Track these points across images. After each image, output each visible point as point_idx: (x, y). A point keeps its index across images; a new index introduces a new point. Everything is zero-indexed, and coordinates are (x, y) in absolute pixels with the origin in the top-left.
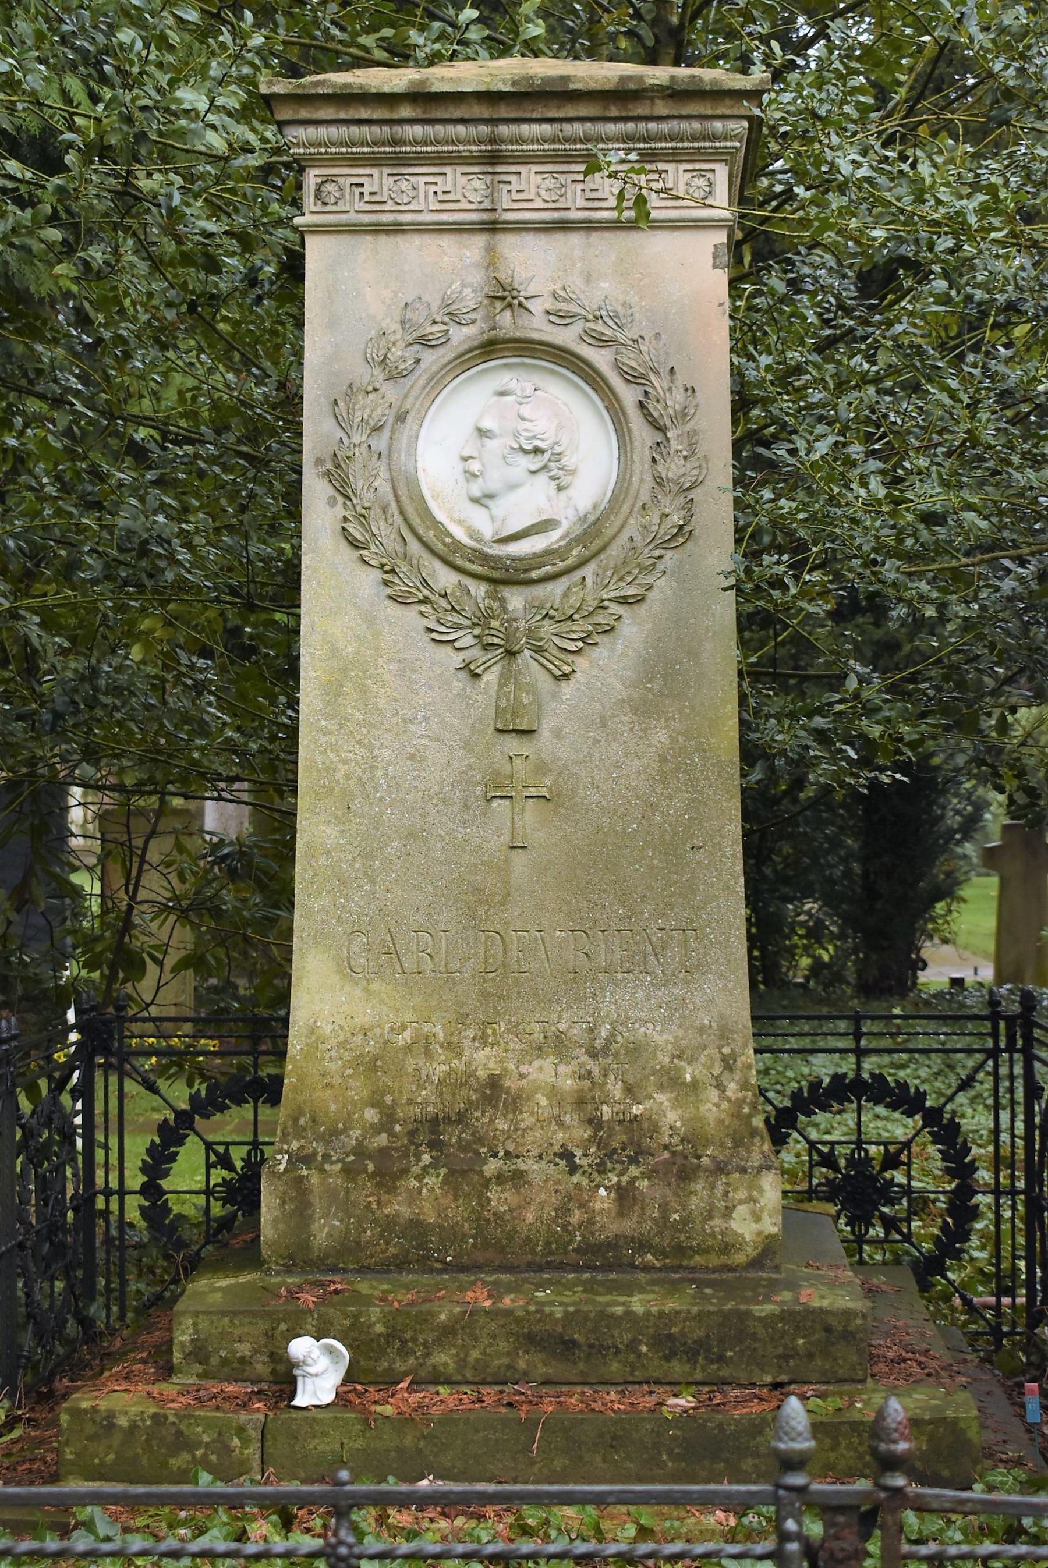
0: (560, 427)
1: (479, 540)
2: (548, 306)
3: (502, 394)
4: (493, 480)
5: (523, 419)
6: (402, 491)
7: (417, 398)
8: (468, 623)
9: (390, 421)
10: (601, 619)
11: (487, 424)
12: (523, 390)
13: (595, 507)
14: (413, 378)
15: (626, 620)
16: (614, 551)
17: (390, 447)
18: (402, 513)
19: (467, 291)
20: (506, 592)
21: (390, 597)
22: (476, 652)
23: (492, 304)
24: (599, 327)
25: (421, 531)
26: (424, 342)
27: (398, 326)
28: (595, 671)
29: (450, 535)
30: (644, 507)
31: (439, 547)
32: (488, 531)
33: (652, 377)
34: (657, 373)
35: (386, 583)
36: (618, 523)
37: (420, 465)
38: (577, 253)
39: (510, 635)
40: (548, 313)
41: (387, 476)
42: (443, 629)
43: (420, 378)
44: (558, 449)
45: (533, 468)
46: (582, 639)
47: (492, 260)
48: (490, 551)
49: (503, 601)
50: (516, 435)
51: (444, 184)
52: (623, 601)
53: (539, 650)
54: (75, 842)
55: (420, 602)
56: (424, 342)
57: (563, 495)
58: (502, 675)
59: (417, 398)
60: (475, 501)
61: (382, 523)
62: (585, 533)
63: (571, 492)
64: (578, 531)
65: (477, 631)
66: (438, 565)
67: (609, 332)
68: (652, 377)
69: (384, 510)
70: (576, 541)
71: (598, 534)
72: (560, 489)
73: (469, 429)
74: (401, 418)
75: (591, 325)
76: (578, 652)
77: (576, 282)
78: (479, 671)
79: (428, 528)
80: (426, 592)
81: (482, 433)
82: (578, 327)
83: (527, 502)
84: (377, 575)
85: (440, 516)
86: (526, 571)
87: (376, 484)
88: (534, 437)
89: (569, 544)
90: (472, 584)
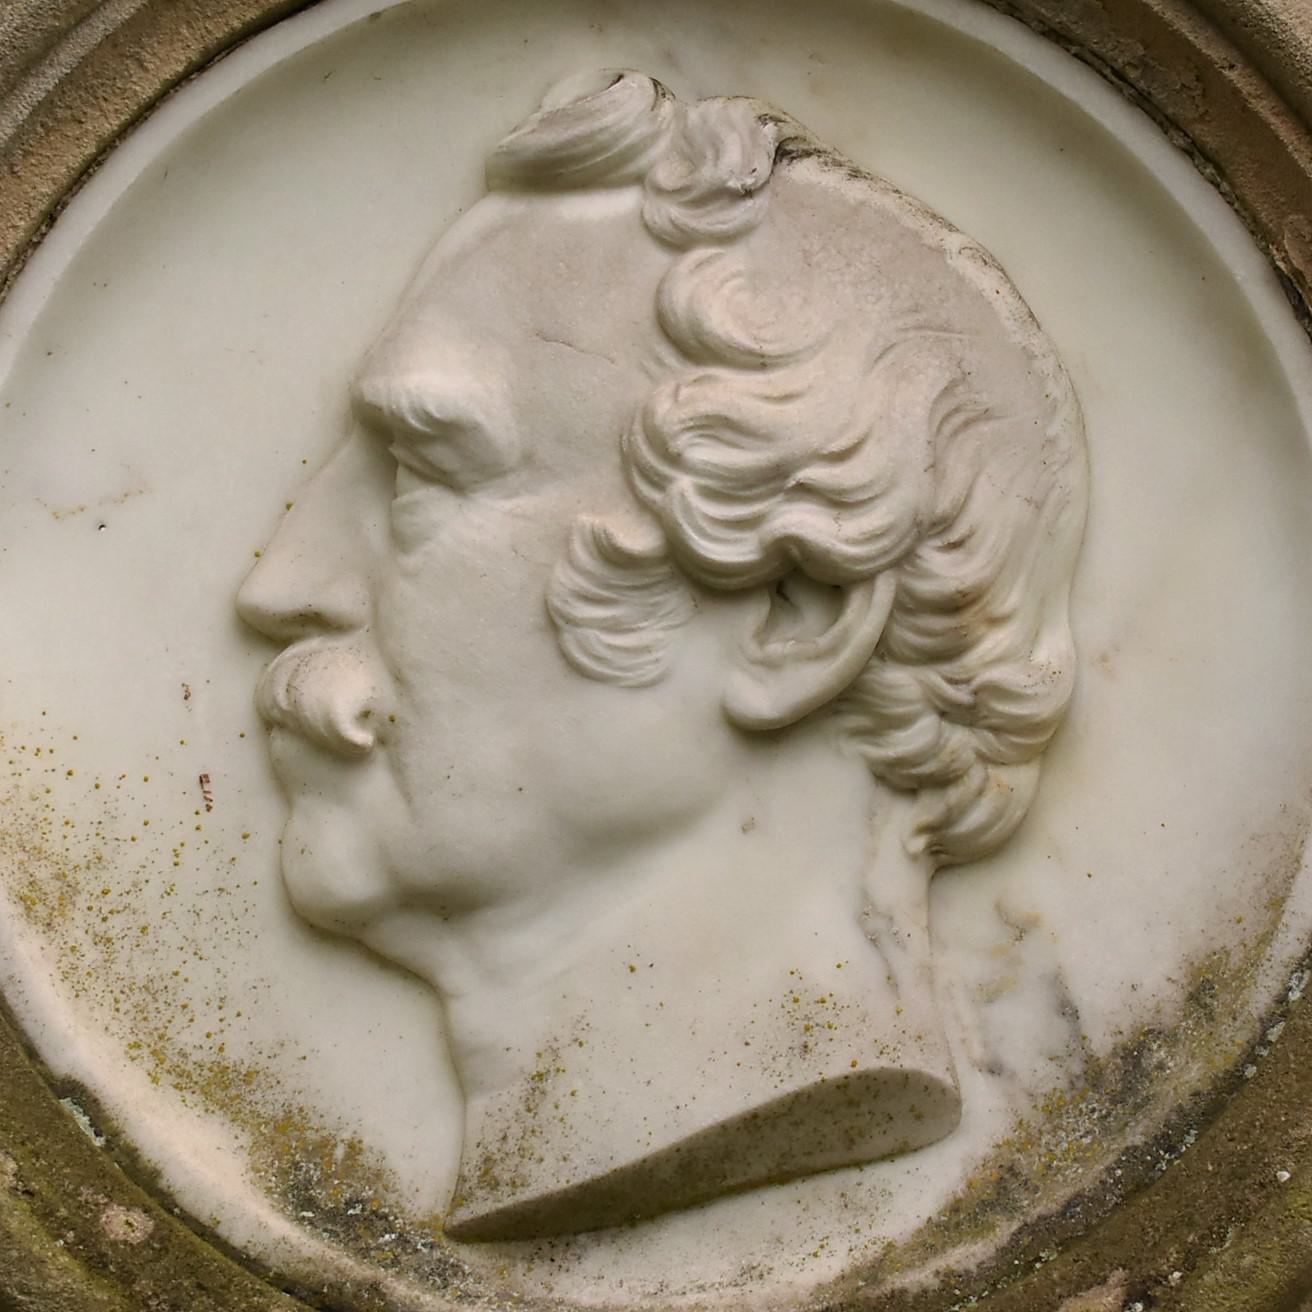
0: (956, 415)
3: (544, 174)
5: (695, 348)
11: (437, 379)
12: (691, 152)
13: (1203, 990)
29: (140, 1180)
44: (943, 572)
45: (763, 700)
50: (644, 461)
51: (600, 1169)
54: (1156, 9)
57: (971, 903)
60: (335, 931)
62: (1138, 1178)
63: (1030, 881)
64: (1081, 1170)
72: (949, 855)
73: (300, 420)
81: (402, 449)
88: (775, 480)
89: (1016, 1259)
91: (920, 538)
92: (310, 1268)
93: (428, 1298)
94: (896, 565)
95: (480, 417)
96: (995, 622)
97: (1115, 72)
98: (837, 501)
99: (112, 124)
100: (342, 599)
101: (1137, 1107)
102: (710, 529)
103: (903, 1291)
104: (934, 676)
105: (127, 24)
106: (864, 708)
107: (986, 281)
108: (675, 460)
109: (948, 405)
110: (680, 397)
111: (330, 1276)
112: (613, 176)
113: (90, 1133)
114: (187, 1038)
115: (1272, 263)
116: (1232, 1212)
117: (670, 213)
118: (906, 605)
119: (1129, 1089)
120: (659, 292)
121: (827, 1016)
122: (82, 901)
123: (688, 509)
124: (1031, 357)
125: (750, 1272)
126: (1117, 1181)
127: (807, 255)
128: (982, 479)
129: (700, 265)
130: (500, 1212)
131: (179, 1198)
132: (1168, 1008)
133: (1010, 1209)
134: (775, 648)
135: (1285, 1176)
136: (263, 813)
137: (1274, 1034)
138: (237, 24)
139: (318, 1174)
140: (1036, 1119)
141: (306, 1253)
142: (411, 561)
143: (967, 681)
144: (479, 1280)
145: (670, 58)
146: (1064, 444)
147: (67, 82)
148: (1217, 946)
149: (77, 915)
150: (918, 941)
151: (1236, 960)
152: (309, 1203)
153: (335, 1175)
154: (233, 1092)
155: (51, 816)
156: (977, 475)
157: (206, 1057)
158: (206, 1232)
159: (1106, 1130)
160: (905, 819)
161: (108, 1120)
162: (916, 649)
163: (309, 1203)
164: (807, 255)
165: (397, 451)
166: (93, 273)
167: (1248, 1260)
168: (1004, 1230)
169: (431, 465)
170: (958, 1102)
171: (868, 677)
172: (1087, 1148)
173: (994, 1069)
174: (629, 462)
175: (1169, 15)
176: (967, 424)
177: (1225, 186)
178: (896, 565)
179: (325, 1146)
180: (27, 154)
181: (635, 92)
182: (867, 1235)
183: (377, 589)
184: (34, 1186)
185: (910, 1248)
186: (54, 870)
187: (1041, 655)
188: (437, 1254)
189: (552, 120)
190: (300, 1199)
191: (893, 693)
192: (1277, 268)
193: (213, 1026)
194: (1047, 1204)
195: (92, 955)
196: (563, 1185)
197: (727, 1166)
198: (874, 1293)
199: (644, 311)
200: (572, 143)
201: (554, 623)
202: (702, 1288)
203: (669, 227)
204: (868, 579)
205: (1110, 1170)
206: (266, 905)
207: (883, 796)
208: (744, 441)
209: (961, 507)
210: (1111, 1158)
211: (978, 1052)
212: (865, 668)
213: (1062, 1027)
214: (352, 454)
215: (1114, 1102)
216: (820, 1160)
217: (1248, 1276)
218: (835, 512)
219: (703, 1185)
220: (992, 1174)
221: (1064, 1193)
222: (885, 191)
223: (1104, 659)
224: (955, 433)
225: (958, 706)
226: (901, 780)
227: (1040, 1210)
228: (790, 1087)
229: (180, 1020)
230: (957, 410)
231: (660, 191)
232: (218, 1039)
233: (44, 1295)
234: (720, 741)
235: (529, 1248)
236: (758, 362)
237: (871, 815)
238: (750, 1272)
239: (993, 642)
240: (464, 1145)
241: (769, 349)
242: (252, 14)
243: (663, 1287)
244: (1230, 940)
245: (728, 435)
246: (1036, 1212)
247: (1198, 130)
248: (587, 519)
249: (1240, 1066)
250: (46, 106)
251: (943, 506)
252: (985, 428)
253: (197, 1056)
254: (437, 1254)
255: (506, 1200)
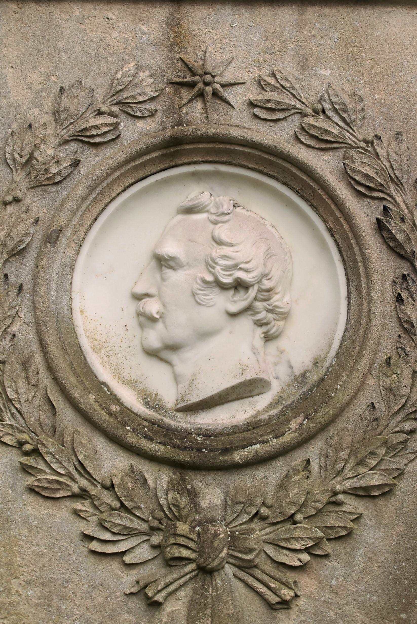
0: (269, 255)
1: (158, 408)
2: (253, 94)
3: (189, 210)
4: (178, 325)
5: (219, 243)
6: (51, 339)
7: (74, 212)
8: (143, 526)
9: (36, 244)
10: (332, 520)
11: (170, 249)
12: (217, 206)
13: (316, 363)
14: (68, 185)
15: (368, 522)
16: (349, 424)
17: (35, 278)
18: (50, 369)
19: (144, 75)
20: (198, 481)
21: (31, 490)
22: (154, 570)
23: (177, 93)
24: (322, 123)
25: (77, 394)
26: (85, 139)
27: (49, 119)
28: (327, 596)
29: (117, 400)
30: (388, 362)
31: (103, 417)
32: (169, 396)
33: (393, 190)
34: (399, 184)
35: (25, 469)
36: (354, 384)
37: (76, 305)
38: (288, 31)
39: (204, 545)
40: (252, 104)
41: (31, 318)
42: (107, 536)
43: (78, 185)
44: (267, 284)
45: (234, 308)
46: (307, 550)
47: (176, 37)
48: (174, 423)
49: (193, 495)
50: (210, 264)
52: (364, 494)
53: (247, 567)
55: (75, 496)
56: (85, 139)
57: (272, 346)
58: (192, 603)
59: (74, 212)
60: (152, 354)
61: (21, 383)
62: (305, 397)
63: (282, 343)
64: (294, 395)
65: (156, 539)
66: (100, 443)
67: (335, 130)
68: (393, 190)
69: (25, 365)
70: (294, 409)
71: (325, 399)
74: (52, 238)
75: (311, 120)
76: (302, 568)
77: (289, 69)
78: (159, 598)
79: (87, 391)
80: (83, 482)
81: (162, 262)
82: (292, 124)
83: (225, 355)
84: (13, 458)
85: (104, 374)
86: (226, 451)
87: (14, 329)
88: (235, 267)
89: (283, 413)
90: (149, 471)
91: (262, 278)
92: (149, 416)
93: (172, 422)
94: (258, 283)
95: (179, 256)
96: (276, 294)
97: (297, 191)
98: (247, 271)
99: (108, 201)
100: (152, 291)
101: (305, 384)
102: (223, 276)
103: (262, 419)
104: (265, 304)
105: (111, 182)
106: (252, 310)
107: (273, 230)
108: (216, 263)
109: (267, 253)
110: (217, 251)
111: (153, 418)
112: (203, 211)
113: (107, 392)
114: (124, 374)
115: (327, 226)
116: (323, 402)
117: (214, 217)
118: (260, 290)
119: (303, 381)
120: (212, 232)
121: (246, 368)
122: (104, 349)
123: (219, 273)
124: (282, 244)
125: (232, 417)
126: (301, 398)
127: (240, 225)
128: (273, 267)
129: (220, 227)
130: (185, 406)
131: (124, 404)
132: (310, 366)
133: (281, 404)
134: (235, 299)
135: (333, 395)
136: (138, 332)
137: (330, 370)
138: (131, 182)
139: (149, 399)
140: (285, 387)
141: (149, 414)
142: (166, 283)
143: (271, 305)
144: (181, 419)
145: (212, 189)
146: (288, 260)
147: (100, 193)
148: (319, 354)
149: (103, 351)
150: (263, 354)
151: (322, 357)
152: (149, 405)
153: (153, 400)
154: (133, 384)
155: (97, 333)
156: (272, 266)
157: (128, 378)
158: (130, 410)
159: (299, 389)
160: (260, 331)
161: (110, 389)
162: (261, 298)
163: (149, 405)
164: (240, 225)
165: (162, 263)
166: (103, 230)
167: (327, 410)
168: (280, 407)
169: (169, 265)
170: (271, 384)
171: (253, 304)
172: (295, 392)
173: (277, 378)
174: (207, 264)
175: (307, 180)
176: (270, 257)
177: (318, 212)
178: (258, 283)
179: (151, 395)
180: (92, 207)
181: (207, 194)
182: (254, 409)
183: (159, 289)
184: (98, 401)
185: (262, 411)
186: (98, 343)
187: (285, 300)
188: (173, 414)
189: (190, 200)
190: (147, 404)
191: (258, 307)
192: (327, 227)
193: (129, 372)
194: (288, 402)
195: (106, 359)
196: (197, 400)
197: (228, 396)
198: (256, 419)
199: (210, 236)
200: (195, 205)
201: (194, 294)
202: (223, 420)
203: (213, 220)
204: (253, 285)
205: (300, 396)
206: (139, 348)
207: (256, 327)
208: (230, 260)
209: (270, 272)
210: (300, 394)
211: (274, 375)
212: (252, 302)
213: (290, 370)
214: (153, 263)
215: (300, 384)
216: (245, 395)
217: (326, 413)
218: (246, 273)
219: (223, 400)
220: (277, 398)
221: (291, 400)
222: (253, 213)
223: (296, 301)
224: (268, 258)
225: (270, 309)
226: (260, 324)
227: (287, 403)
228: (240, 381)
229: (123, 371)
230: (269, 254)
231: (211, 213)
232: (130, 375)
233: (102, 420)
234: (225, 316)
235: (190, 413)
236: (232, 245)
237: (254, 330)
238: (232, 417)
239: (276, 298)
240: (177, 394)
241: (233, 243)
242: (134, 180)
243: (216, 420)
244: (321, 353)
245: (226, 259)
246: (286, 404)
247: (312, 201)
248: (199, 275)
249: (324, 376)
250: (95, 198)
251: (267, 272)
252: (274, 257)
253: (126, 378)
254: (173, 414)
255: (186, 403)
